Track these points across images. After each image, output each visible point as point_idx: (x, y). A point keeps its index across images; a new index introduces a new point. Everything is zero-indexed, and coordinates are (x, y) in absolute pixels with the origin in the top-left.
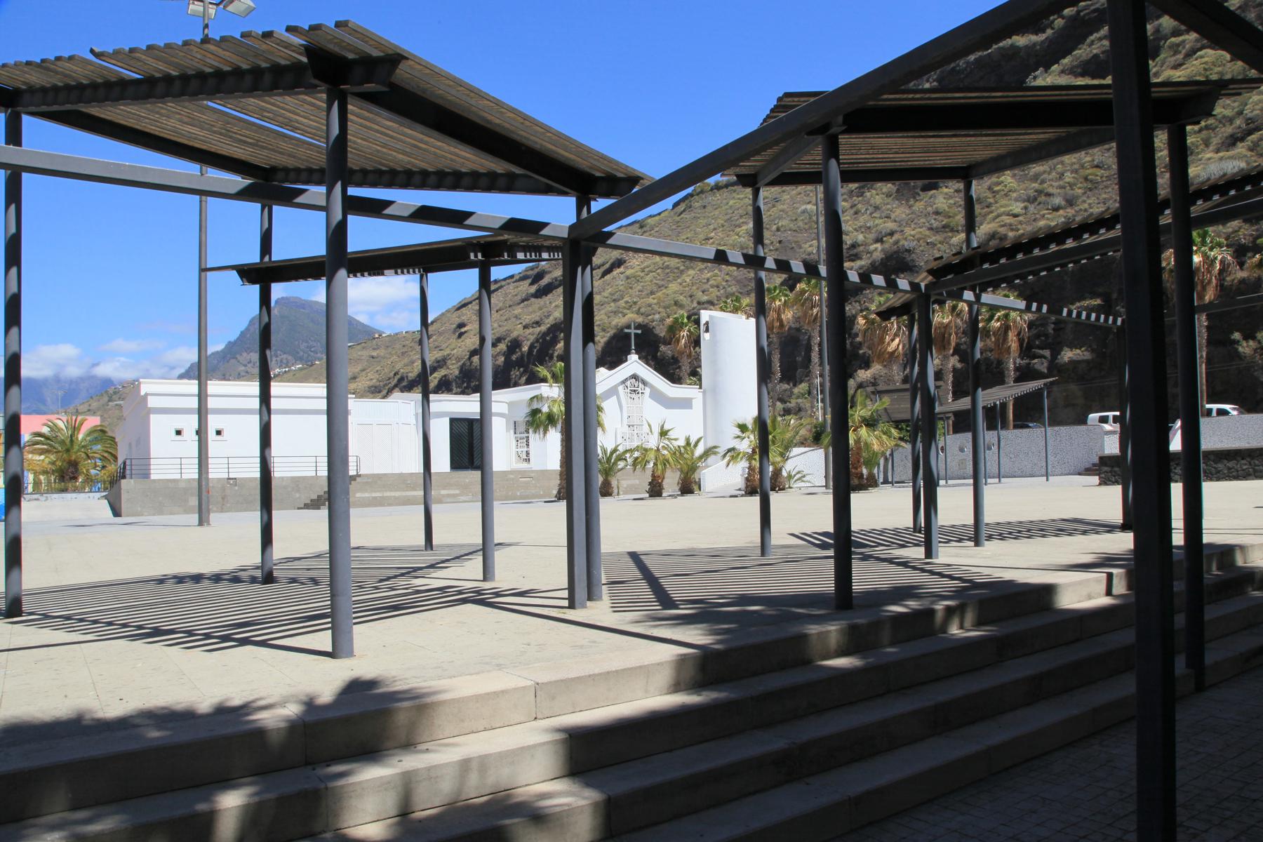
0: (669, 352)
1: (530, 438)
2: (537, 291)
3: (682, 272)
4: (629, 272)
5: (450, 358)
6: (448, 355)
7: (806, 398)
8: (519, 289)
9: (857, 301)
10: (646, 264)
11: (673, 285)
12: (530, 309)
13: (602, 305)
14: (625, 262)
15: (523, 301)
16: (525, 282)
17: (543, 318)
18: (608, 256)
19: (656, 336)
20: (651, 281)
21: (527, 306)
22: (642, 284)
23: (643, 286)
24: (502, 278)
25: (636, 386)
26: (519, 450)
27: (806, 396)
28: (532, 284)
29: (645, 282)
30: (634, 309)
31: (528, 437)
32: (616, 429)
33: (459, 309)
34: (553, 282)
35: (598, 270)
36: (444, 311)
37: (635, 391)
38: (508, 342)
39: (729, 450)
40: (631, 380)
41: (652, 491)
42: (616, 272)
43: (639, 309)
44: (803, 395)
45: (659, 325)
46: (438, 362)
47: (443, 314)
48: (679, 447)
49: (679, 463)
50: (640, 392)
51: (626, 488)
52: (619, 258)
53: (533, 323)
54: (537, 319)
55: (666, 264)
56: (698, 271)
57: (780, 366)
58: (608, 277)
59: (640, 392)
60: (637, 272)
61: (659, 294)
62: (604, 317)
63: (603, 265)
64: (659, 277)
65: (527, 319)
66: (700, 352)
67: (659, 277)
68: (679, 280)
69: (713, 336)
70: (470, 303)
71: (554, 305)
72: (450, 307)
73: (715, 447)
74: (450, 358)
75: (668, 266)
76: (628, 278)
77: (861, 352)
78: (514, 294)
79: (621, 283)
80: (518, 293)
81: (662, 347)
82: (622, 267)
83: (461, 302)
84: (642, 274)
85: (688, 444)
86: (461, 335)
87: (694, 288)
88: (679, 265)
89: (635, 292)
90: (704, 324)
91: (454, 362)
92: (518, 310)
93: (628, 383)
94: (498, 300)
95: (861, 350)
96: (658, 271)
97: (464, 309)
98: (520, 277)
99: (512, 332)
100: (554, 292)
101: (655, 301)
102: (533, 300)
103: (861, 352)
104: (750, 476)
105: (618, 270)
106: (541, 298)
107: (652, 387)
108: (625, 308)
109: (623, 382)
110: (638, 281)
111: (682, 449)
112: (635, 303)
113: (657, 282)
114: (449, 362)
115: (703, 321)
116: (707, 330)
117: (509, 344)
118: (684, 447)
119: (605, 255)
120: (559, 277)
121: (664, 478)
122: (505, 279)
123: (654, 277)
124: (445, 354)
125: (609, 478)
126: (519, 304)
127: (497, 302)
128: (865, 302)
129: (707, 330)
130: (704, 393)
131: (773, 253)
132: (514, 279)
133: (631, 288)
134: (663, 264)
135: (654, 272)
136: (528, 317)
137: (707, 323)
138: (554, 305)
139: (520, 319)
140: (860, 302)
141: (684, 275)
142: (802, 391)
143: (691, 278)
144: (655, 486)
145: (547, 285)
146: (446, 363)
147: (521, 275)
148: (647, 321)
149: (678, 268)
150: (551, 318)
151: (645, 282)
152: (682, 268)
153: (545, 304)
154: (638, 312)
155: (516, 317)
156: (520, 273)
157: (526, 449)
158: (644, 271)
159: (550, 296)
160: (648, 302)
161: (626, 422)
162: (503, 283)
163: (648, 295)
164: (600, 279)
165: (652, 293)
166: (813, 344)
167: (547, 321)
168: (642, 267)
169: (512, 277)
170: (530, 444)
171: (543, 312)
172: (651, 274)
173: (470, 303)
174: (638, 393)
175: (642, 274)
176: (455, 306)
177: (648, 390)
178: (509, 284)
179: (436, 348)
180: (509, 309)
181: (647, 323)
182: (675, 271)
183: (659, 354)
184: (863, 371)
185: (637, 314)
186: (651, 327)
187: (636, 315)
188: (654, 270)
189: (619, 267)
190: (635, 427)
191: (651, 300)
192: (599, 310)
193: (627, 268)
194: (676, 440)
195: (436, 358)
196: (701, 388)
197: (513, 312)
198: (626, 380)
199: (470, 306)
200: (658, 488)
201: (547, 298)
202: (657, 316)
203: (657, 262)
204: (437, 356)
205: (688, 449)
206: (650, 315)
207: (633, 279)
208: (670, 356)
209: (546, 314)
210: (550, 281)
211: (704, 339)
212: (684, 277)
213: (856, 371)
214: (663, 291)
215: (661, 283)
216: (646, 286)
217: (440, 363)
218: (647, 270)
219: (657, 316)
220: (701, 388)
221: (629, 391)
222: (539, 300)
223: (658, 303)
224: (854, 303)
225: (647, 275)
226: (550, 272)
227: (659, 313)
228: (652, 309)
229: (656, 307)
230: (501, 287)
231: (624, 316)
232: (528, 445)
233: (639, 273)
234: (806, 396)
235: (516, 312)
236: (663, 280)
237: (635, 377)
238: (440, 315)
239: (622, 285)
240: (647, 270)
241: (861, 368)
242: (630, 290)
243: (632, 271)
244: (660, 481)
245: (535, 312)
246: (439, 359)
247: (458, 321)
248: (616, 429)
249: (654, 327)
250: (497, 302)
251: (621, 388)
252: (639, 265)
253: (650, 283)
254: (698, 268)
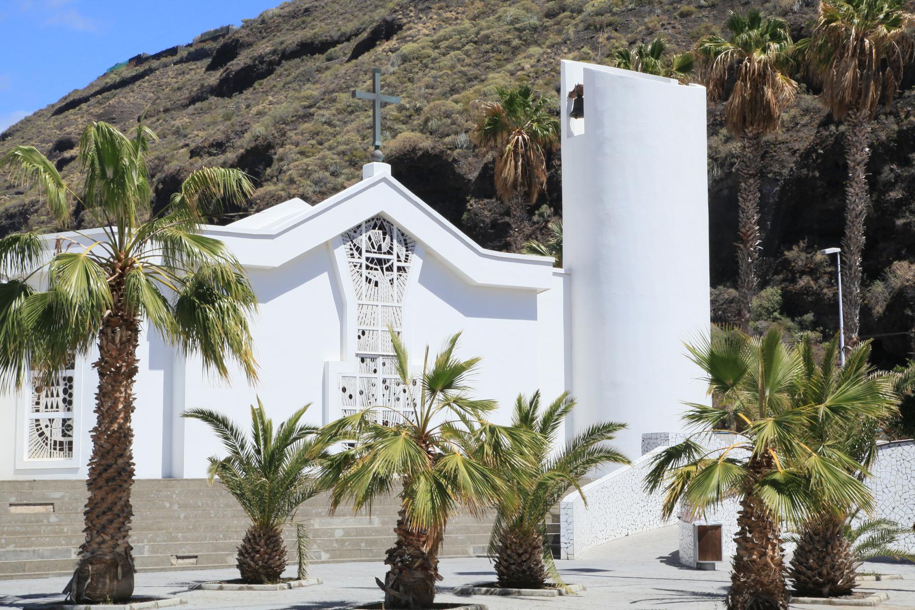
0: (486, 213)
1: (75, 383)
2: (223, 81)
3: (515, 50)
4: (407, 48)
5: (36, 211)
6: (33, 204)
7: (775, 319)
8: (188, 77)
9: (891, 113)
10: (441, 33)
11: (496, 75)
12: (207, 118)
13: (352, 112)
14: (400, 27)
15: (193, 101)
16: (199, 64)
17: (233, 135)
18: (366, 17)
19: (460, 177)
20: (452, 67)
21: (202, 112)
22: (433, 72)
23: (435, 78)
24: (152, 53)
25: (385, 248)
26: (44, 416)
27: (776, 314)
28: (211, 68)
29: (440, 69)
30: (415, 122)
31: (70, 379)
32: (326, 365)
33: (60, 111)
34: (255, 66)
35: (345, 44)
36: (30, 113)
37: (380, 262)
38: (159, 181)
39: (673, 454)
40: (371, 233)
41: (395, 587)
42: (383, 47)
43: (427, 120)
44: (769, 313)
45: (466, 157)
46: (11, 216)
47: (27, 120)
48: (493, 430)
49: (494, 488)
50: (396, 264)
51: (341, 542)
52: (389, 18)
53: (212, 146)
54: (220, 137)
55: (482, 33)
56: (549, 47)
57: (758, 223)
58: (365, 57)
59: (396, 264)
60: (423, 48)
61: (469, 93)
62: (355, 137)
63: (356, 35)
64: (468, 60)
65: (199, 137)
66: (560, 165)
67: (468, 60)
68: (510, 67)
69: (594, 128)
70: (85, 100)
71: (254, 110)
72: (44, 107)
73: (606, 430)
74: (36, 211)
75: (487, 37)
76: (405, 59)
77: (900, 222)
78: (176, 86)
79: (392, 69)
80: (184, 85)
81: (472, 202)
82: (395, 37)
83: (65, 98)
84: (434, 54)
85: (526, 418)
86: (61, 165)
87: (540, 82)
88: (509, 36)
89: (418, 88)
90: (571, 95)
91: (43, 218)
92: (181, 120)
93: (363, 240)
94: (144, 98)
95: (899, 218)
96: (467, 47)
97: (71, 111)
98: (189, 54)
99: (167, 163)
100: (256, 85)
101: (459, 107)
102: (213, 99)
103: (900, 222)
104: (750, 552)
105: (387, 45)
106: (230, 97)
107: (428, 255)
108: (396, 119)
109: (350, 236)
110: (427, 67)
111: (506, 441)
112: (418, 110)
113: (463, 69)
114: (33, 218)
115: (568, 87)
116: (578, 112)
117: (161, 186)
118: (510, 432)
119: (361, 14)
120: (267, 54)
121: (439, 539)
122: (157, 56)
123: (459, 60)
124: (27, 201)
125: (274, 521)
126: (186, 106)
127: (141, 102)
128: (908, 115)
129: (578, 112)
130: (568, 277)
131: (705, 13)
132: (176, 58)
133: (411, 80)
134: (477, 33)
135: (458, 49)
136: (201, 134)
137: (578, 92)
138: (254, 110)
139: (185, 136)
140: (896, 115)
141: (520, 57)
142: (766, 304)
143: (533, 61)
144: (407, 567)
145: (242, 69)
146: (26, 220)
147: (192, 49)
148: (442, 147)
149: (507, 43)
150: (247, 136)
151: (440, 69)
152: (516, 42)
153: (238, 108)
154: (424, 128)
155: (177, 132)
156: (190, 45)
157: (61, 414)
158: (437, 48)
159: (248, 93)
160: (443, 109)
161: (353, 346)
162: (155, 64)
163: (445, 93)
164: (349, 61)
165: (453, 90)
166: (851, 164)
167: (238, 143)
168: (435, 38)
169: (173, 51)
170: (75, 399)
171: (233, 125)
172: (452, 53)
173: (85, 100)
174: (390, 269)
175: (434, 54)
176: (53, 106)
177: (415, 263)
178: (166, 66)
179: (8, 188)
180: (163, 115)
181: (442, 152)
182: (502, 47)
183: (465, 216)
184: (905, 264)
185: (421, 131)
186: (450, 160)
187: (419, 134)
188: (459, 45)
189: (388, 38)
190: (380, 360)
191: (449, 104)
192: (345, 123)
193: (404, 40)
194: (486, 405)
195: (7, 210)
196: (559, 264)
197: (173, 123)
198: (357, 229)
199: (84, 106)
200: (419, 575)
201: (243, 96)
202: (462, 138)
203: (466, 30)
204: (8, 205)
205: (525, 438)
206: (448, 135)
207: (415, 62)
208: (488, 220)
209: (238, 128)
210: (249, 62)
211: (570, 134)
212: (520, 59)
213: (890, 263)
214: (477, 87)
215: (472, 71)
216: (440, 76)
217: (16, 220)
218: (444, 44)
219: (462, 138)
220: (559, 264)
221: (364, 262)
222: (227, 100)
223: (465, 111)
224: (883, 117)
225: (444, 55)
226: (250, 45)
227: (466, 132)
228: (453, 123)
229: (461, 120)
230: (151, 71)
231: (394, 137)
232: (68, 403)
233: (429, 51)
234: (776, 314)
235: (178, 123)
236: (476, 65)
237: (380, 223)
238: (22, 122)
239: (394, 73)
240: (444, 44)
241: (900, 258)
242: (409, 84)
243: (415, 45)
244: (425, 549)
245: (215, 123)
246: (12, 211)
247: (57, 135)
248: (326, 365)
249: (455, 161)
250: (141, 102)
251: (341, 253)
252: (427, 35)
253: (449, 72)
254: (548, 43)
